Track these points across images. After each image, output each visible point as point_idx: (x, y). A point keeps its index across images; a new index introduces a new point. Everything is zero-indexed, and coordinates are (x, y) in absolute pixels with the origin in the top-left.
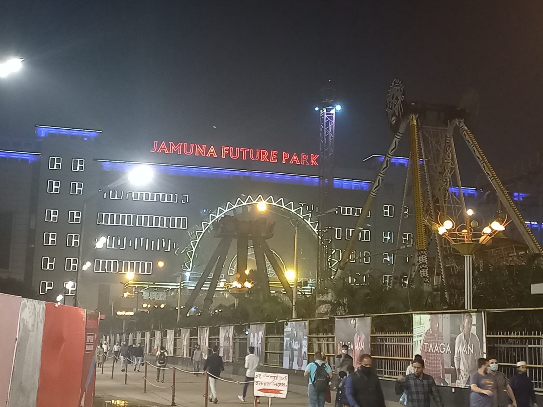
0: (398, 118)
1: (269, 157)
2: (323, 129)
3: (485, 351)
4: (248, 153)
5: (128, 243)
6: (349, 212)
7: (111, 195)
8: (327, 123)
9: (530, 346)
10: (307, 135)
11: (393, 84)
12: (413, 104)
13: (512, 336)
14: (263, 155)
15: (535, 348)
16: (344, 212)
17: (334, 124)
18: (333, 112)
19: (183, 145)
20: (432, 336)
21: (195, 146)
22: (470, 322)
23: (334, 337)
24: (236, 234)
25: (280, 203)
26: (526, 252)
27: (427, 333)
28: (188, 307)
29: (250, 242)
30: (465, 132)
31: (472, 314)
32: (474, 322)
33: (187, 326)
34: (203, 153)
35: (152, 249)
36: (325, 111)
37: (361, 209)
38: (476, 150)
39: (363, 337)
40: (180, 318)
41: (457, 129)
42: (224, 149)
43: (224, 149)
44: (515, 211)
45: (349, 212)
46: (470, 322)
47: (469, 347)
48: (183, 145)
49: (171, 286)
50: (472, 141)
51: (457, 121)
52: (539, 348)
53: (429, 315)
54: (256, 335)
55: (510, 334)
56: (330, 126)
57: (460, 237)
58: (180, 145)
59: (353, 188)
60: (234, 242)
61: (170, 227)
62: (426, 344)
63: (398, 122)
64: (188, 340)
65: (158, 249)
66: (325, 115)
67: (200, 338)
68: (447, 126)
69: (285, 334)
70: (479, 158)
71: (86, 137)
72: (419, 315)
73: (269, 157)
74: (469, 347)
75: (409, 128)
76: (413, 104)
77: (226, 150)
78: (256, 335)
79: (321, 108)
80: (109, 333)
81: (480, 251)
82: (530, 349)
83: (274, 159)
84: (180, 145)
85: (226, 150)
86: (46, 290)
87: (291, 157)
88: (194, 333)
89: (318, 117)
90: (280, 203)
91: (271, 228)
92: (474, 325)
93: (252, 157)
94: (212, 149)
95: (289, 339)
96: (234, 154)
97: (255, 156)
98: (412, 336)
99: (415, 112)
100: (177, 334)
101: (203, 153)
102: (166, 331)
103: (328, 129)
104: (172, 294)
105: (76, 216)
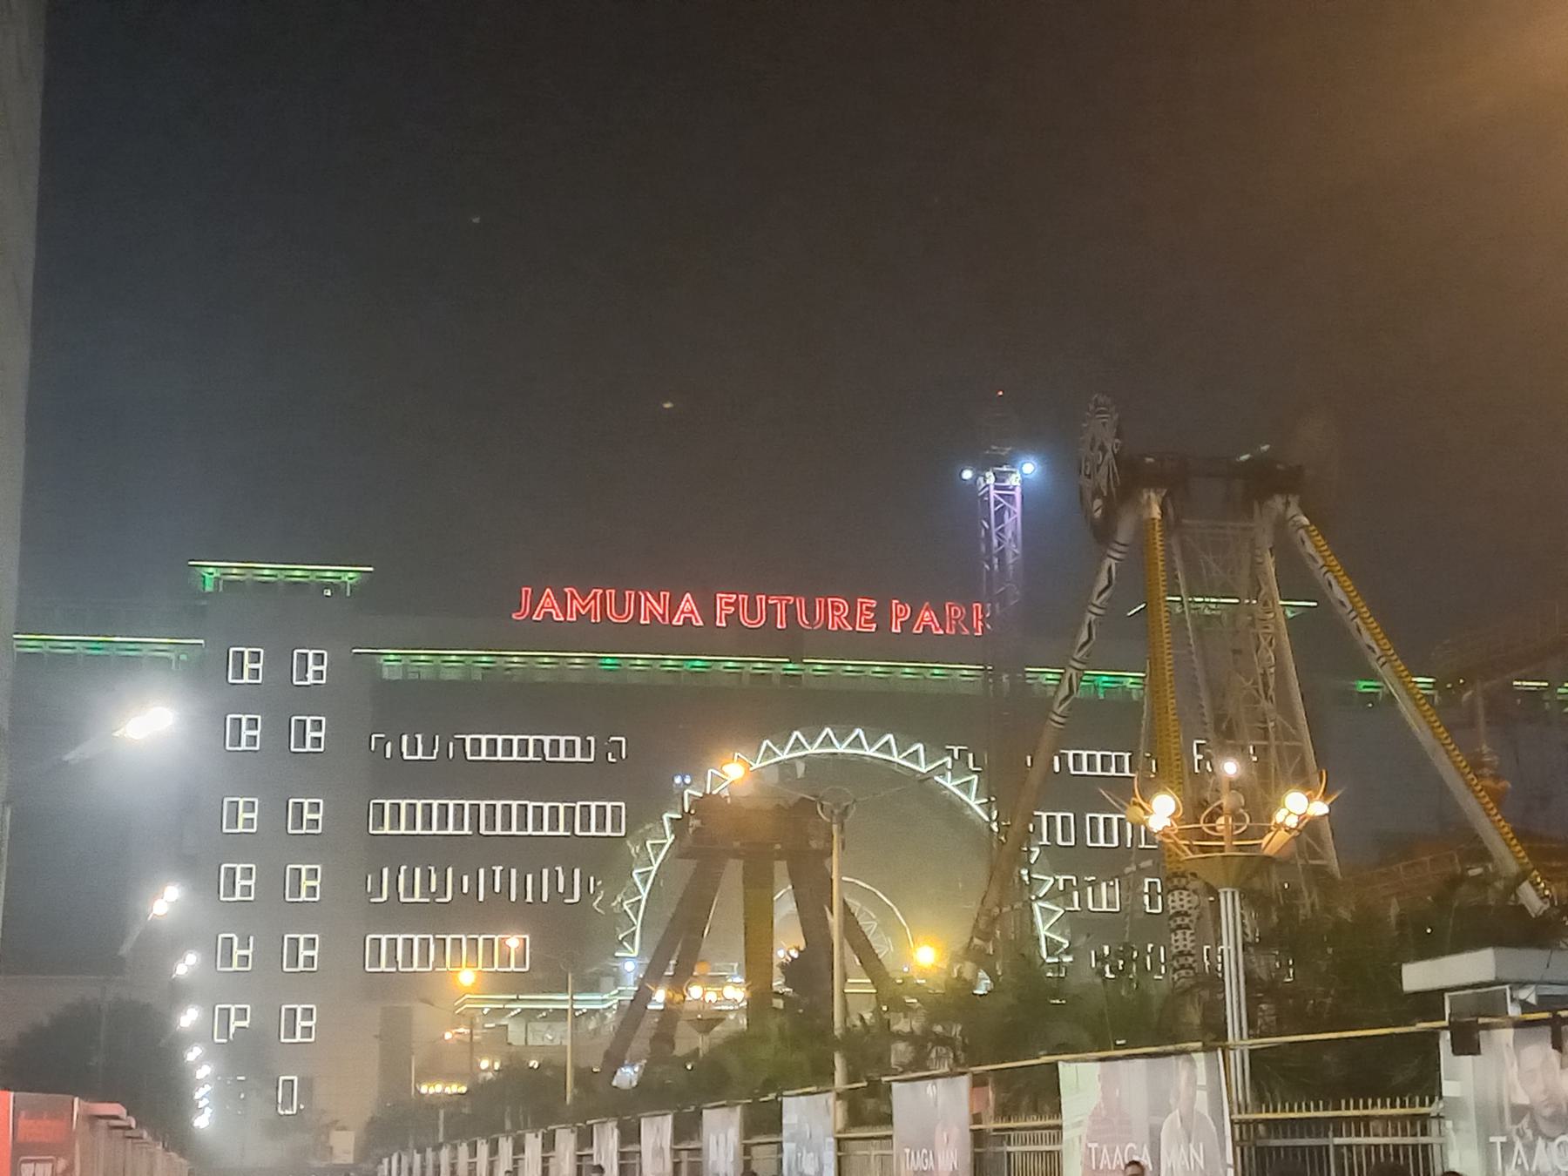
0: (1107, 501)
1: (851, 618)
2: (988, 532)
3: (1230, 1160)
4: (791, 610)
5: (458, 883)
6: (1091, 766)
7: (404, 749)
8: (1000, 519)
9: (1338, 1141)
10: (934, 550)
11: (1092, 407)
12: (1149, 460)
13: (1379, 1111)
14: (835, 614)
15: (1415, 1146)
16: (1077, 766)
17: (1019, 515)
18: (1014, 480)
19: (603, 596)
20: (1108, 1122)
21: (638, 599)
22: (1192, 1080)
23: (890, 1137)
24: (737, 844)
25: (886, 748)
26: (1486, 868)
27: (1094, 1114)
28: (614, 1060)
29: (781, 867)
30: (1302, 532)
31: (1194, 1055)
32: (1202, 1080)
33: (606, 1112)
34: (663, 617)
35: (529, 899)
36: (991, 480)
37: (1127, 756)
38: (1333, 582)
39: (955, 1131)
40: (574, 1097)
41: (1281, 524)
42: (722, 598)
43: (722, 598)
44: (1447, 752)
45: (1091, 766)
46: (1192, 1080)
47: (1192, 1150)
48: (603, 596)
49: (587, 1002)
50: (1324, 557)
51: (1278, 502)
52: (1425, 1146)
53: (1098, 1064)
54: (722, 1137)
55: (1374, 1104)
56: (1007, 520)
57: (1209, 838)
58: (594, 597)
59: (1102, 696)
60: (733, 873)
61: (578, 832)
62: (1093, 1146)
63: (1110, 514)
64: (573, 1159)
65: (545, 899)
66: (993, 493)
67: (599, 1152)
68: (1251, 517)
69: (785, 1133)
70: (1342, 603)
71: (327, 586)
72: (1073, 1065)
73: (851, 618)
74: (1192, 1150)
75: (1144, 527)
76: (1149, 460)
77: (727, 604)
78: (722, 1137)
79: (980, 470)
80: (404, 1148)
81: (1253, 877)
82: (1338, 1147)
83: (867, 621)
84: (594, 597)
85: (727, 604)
86: (232, 1030)
87: (915, 614)
88: (687, 1129)
89: (973, 500)
90: (886, 748)
91: (1266, 787)
92: (1201, 1087)
93: (803, 621)
94: (688, 603)
95: (793, 1145)
96: (752, 614)
97: (811, 615)
98: (1059, 1127)
99: (1154, 481)
100: (549, 1144)
101: (663, 617)
102: (523, 1136)
103: (1002, 530)
104: (592, 1025)
105: (311, 811)
